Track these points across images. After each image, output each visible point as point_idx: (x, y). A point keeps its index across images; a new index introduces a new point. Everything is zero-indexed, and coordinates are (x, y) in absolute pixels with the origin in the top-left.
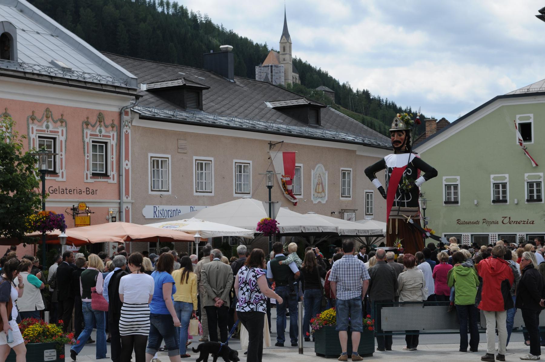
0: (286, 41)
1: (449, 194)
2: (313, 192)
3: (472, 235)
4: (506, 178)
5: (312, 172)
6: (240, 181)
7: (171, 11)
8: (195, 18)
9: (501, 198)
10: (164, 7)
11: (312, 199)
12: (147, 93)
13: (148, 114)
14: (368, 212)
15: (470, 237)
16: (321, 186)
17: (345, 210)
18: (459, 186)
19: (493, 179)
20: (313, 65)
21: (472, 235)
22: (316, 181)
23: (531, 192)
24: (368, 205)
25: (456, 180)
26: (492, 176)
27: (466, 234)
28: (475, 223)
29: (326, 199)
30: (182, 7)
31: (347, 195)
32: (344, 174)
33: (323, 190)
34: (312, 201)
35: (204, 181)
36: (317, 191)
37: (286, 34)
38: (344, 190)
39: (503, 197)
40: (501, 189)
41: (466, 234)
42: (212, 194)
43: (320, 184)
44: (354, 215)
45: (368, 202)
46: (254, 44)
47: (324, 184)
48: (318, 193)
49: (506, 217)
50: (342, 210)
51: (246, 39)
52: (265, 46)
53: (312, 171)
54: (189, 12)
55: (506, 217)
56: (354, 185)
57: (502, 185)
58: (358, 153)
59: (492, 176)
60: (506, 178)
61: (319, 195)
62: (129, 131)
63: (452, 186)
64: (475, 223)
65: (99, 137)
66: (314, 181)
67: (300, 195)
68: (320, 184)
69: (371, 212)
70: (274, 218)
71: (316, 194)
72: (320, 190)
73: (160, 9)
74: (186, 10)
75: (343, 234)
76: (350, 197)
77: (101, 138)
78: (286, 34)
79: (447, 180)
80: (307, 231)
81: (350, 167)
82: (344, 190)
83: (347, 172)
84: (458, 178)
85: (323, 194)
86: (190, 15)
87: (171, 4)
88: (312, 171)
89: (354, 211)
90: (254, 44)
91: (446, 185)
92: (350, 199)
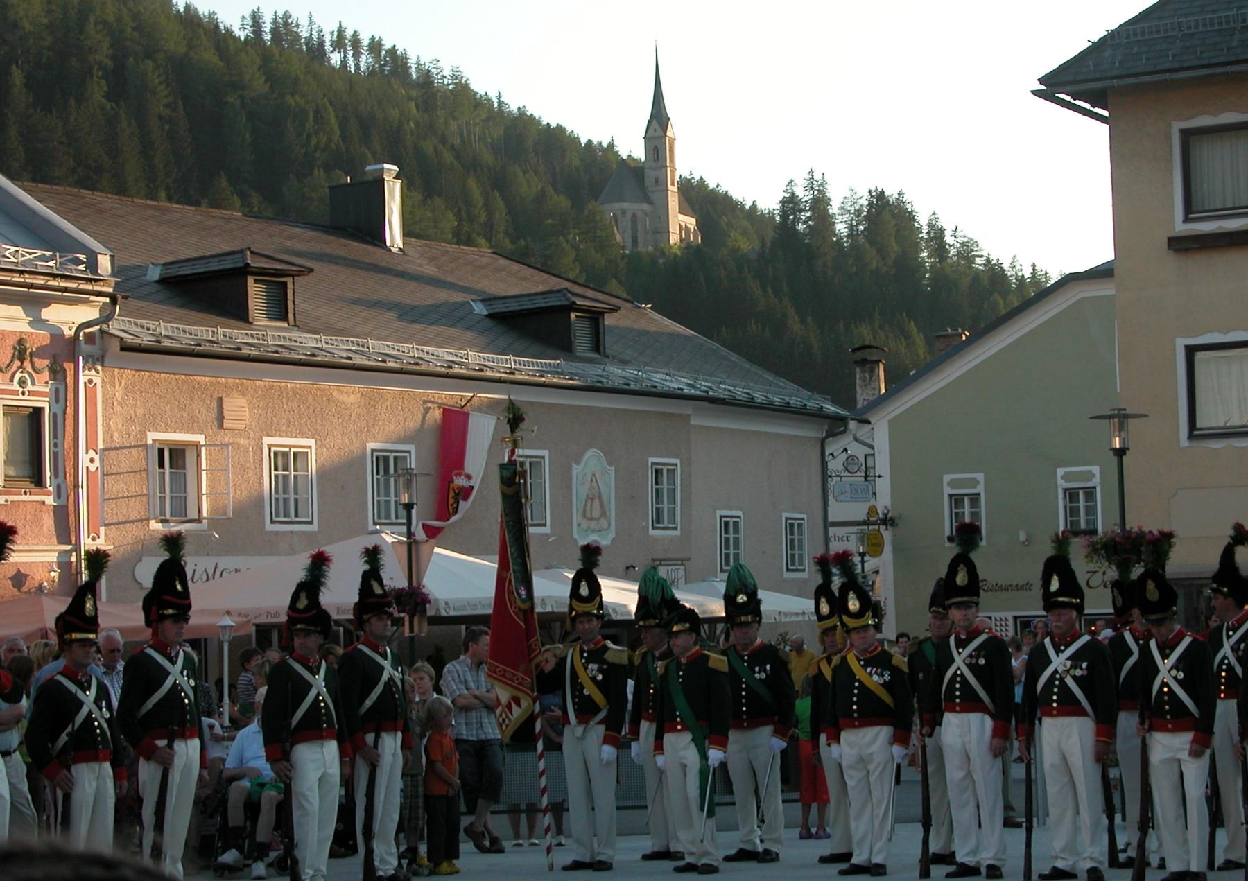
0: (660, 132)
1: (1074, 512)
2: (576, 518)
3: (1015, 618)
4: (1094, 475)
5: (576, 469)
6: (387, 494)
7: (365, 60)
8: (426, 76)
9: (1083, 526)
10: (345, 52)
11: (576, 535)
12: (158, 287)
13: (146, 340)
14: (793, 564)
15: (1011, 623)
16: (597, 502)
17: (661, 560)
18: (1098, 489)
19: (1062, 478)
20: (736, 195)
21: (1015, 618)
22: (584, 491)
23: (1074, 512)
24: (727, 548)
25: (975, 483)
26: (1061, 471)
27: (1003, 615)
28: (1022, 588)
29: (612, 535)
30: (392, 51)
31: (666, 524)
32: (658, 473)
33: (604, 513)
34: (575, 540)
35: (292, 496)
36: (588, 515)
37: (659, 117)
38: (659, 512)
39: (1087, 522)
40: (1082, 503)
41: (1003, 615)
42: (314, 527)
43: (594, 496)
44: (681, 573)
45: (727, 540)
46: (583, 141)
47: (605, 498)
48: (592, 519)
49: (1095, 572)
50: (653, 560)
51: (560, 129)
52: (611, 145)
53: (574, 466)
54: (412, 62)
55: (1095, 572)
56: (686, 499)
57: (971, 500)
58: (694, 421)
59: (1061, 471)
60: (1062, 478)
61: (593, 524)
62: (97, 380)
63: (1081, 493)
64: (1022, 588)
65: (21, 397)
66: (579, 491)
67: (545, 525)
68: (594, 496)
69: (801, 564)
70: (419, 583)
71: (585, 524)
72: (596, 513)
73: (335, 59)
74: (405, 59)
75: (444, 613)
76: (676, 529)
77: (26, 397)
78: (659, 117)
79: (952, 484)
80: (619, 618)
81: (677, 457)
82: (659, 512)
83: (665, 469)
84: (980, 476)
85: (604, 523)
86: (413, 70)
87: (366, 42)
88: (574, 466)
89: (682, 561)
90: (583, 141)
91: (951, 496)
92: (678, 533)
